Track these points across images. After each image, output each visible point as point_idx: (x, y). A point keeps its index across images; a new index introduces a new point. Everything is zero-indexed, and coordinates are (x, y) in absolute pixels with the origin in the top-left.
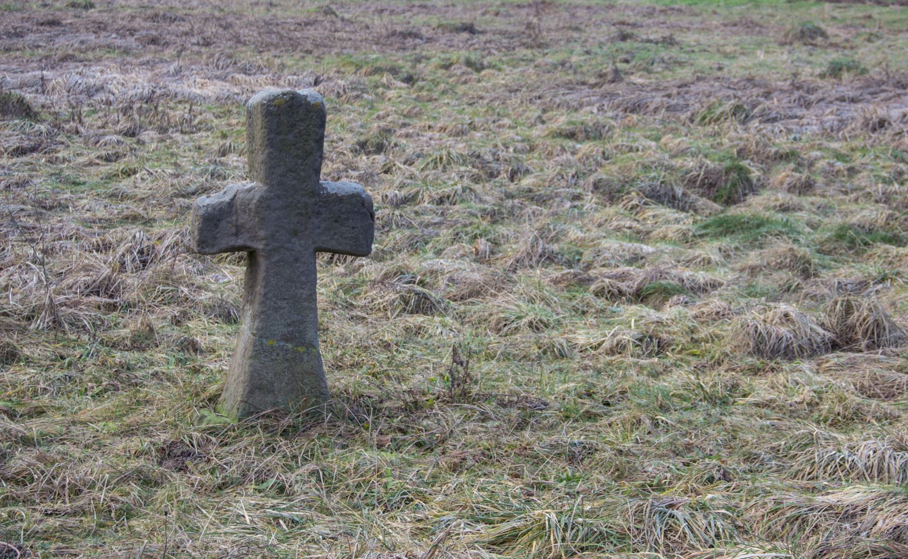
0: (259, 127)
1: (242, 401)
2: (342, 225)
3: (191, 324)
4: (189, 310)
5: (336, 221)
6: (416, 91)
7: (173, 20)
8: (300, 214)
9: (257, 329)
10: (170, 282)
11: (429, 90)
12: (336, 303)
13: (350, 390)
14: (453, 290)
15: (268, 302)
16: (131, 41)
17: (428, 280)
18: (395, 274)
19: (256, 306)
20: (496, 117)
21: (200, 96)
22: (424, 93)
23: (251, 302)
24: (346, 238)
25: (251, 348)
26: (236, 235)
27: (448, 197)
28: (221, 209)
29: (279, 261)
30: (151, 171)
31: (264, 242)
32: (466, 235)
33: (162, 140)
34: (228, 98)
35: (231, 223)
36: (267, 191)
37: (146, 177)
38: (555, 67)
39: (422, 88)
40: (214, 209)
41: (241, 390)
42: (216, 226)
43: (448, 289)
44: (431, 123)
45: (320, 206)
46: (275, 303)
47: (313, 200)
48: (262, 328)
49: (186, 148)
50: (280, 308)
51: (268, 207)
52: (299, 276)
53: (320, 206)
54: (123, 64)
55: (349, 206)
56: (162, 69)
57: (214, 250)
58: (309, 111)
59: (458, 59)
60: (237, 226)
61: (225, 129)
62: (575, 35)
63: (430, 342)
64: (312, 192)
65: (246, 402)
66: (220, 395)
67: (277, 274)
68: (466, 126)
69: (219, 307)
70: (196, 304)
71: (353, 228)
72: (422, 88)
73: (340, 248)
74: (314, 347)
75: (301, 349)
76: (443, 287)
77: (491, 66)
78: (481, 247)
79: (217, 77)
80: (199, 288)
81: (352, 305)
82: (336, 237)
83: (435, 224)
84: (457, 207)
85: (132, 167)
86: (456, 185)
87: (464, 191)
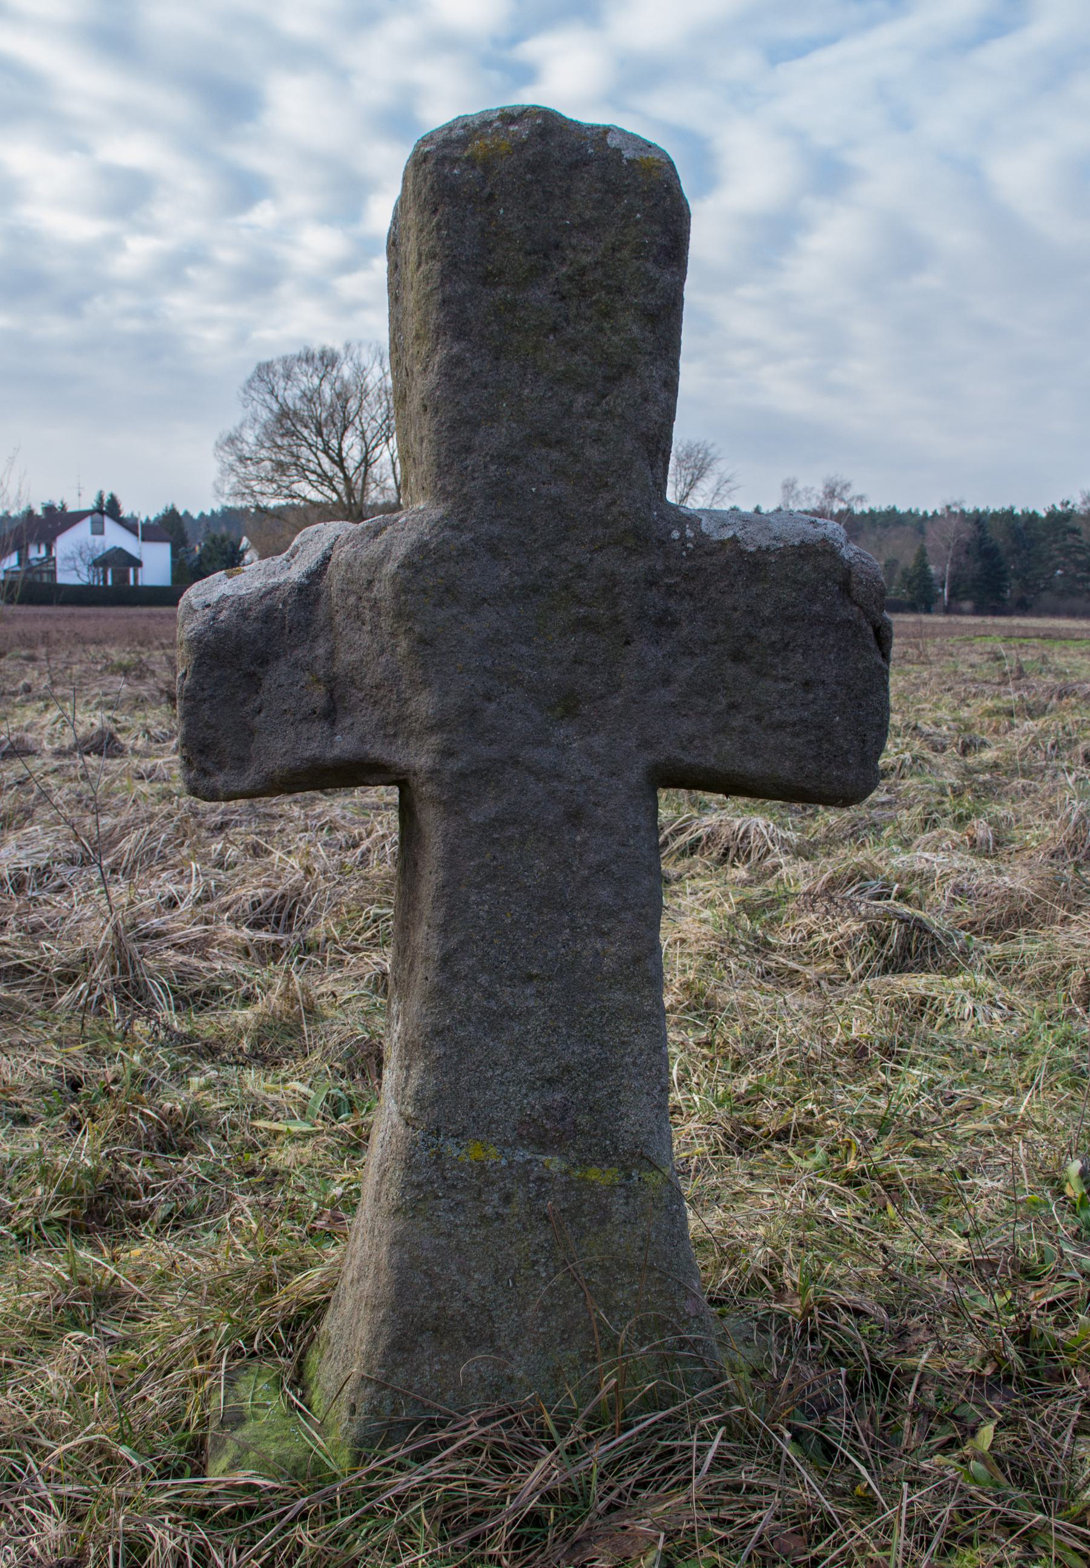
1: (365, 1381)
5: (738, 657)
8: (584, 624)
9: (418, 1099)
12: (733, 941)
14: (967, 911)
19: (415, 1005)
24: (780, 726)
26: (330, 714)
27: (893, 769)
28: (269, 616)
29: (499, 822)
31: (434, 741)
35: (308, 668)
36: (444, 523)
41: (363, 1332)
42: (253, 681)
43: (958, 909)
45: (670, 591)
46: (490, 995)
47: (640, 565)
48: (439, 1098)
51: (449, 591)
53: (670, 591)
57: (246, 783)
71: (807, 685)
73: (753, 766)
74: (654, 1167)
75: (600, 1176)
78: (980, 834)
82: (737, 721)
83: (883, 804)
84: (908, 782)
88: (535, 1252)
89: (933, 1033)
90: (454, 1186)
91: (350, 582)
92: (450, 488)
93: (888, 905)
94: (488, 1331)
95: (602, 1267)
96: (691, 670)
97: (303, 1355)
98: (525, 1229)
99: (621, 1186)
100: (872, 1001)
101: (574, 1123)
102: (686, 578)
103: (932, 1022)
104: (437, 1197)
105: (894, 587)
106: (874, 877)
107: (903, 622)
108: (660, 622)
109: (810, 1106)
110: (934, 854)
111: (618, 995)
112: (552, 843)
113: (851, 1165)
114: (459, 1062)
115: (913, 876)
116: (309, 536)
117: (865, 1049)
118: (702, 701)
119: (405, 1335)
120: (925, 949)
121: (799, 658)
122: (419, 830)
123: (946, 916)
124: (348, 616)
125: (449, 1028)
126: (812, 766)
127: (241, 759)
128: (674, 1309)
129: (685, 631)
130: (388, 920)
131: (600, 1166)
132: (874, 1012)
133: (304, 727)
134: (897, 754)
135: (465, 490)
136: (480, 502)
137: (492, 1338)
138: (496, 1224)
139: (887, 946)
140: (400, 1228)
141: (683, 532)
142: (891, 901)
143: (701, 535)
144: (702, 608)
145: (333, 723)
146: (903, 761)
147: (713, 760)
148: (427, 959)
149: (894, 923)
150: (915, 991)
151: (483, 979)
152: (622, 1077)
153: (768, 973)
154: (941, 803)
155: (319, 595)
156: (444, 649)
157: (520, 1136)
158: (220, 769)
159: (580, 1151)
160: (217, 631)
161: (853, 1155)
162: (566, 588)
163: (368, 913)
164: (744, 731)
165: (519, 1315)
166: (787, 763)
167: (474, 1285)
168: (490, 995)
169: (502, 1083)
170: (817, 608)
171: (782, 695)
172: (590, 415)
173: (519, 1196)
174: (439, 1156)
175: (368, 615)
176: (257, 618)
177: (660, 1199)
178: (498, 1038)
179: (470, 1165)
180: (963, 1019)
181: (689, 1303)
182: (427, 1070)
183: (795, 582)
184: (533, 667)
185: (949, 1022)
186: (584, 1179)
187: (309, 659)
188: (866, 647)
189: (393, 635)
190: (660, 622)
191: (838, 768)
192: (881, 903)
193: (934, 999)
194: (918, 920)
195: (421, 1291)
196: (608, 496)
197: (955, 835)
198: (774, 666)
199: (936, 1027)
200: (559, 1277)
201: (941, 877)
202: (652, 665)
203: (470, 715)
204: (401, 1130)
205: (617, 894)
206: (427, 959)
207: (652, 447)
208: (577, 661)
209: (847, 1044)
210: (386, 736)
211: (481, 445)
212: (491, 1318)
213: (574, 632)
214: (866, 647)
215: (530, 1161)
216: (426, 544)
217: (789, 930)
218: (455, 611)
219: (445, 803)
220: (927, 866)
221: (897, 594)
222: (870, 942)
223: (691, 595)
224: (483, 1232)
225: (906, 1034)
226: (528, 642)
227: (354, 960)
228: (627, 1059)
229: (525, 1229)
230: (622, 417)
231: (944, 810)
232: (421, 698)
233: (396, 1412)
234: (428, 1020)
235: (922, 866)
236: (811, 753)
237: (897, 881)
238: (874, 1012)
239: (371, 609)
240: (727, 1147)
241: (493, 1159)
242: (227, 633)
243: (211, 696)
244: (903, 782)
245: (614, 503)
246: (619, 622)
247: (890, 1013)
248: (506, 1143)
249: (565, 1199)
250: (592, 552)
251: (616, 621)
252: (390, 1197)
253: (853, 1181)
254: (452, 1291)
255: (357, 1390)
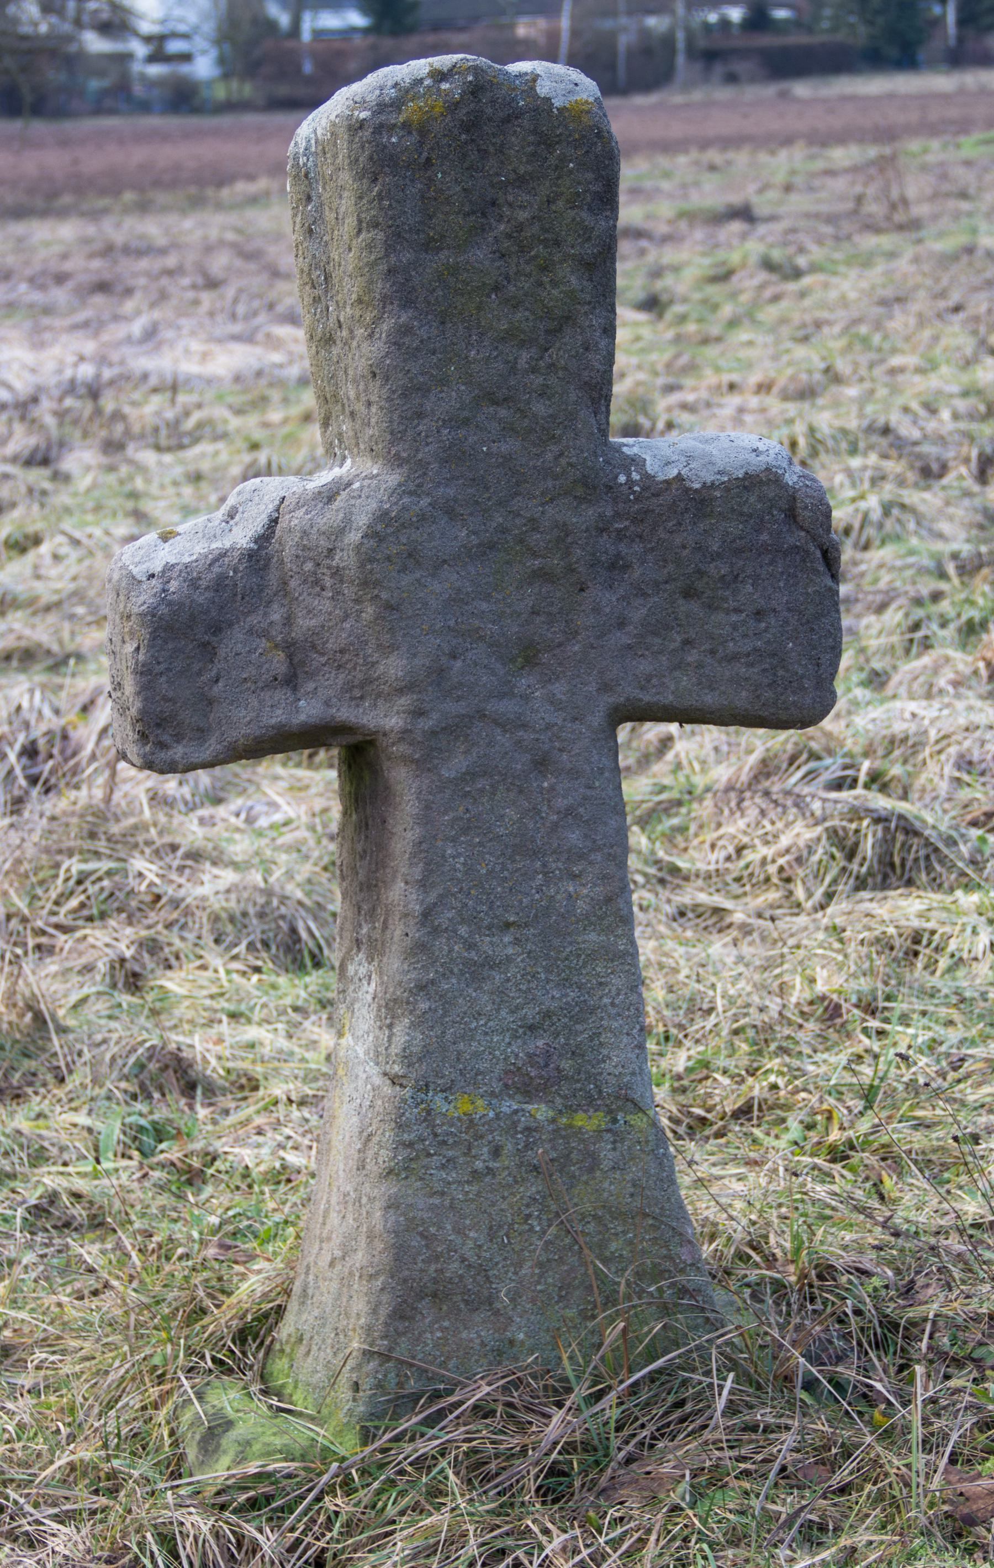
0: (351, 222)
1: (367, 1355)
2: (711, 607)
3: (173, 983)
4: (165, 936)
5: (689, 593)
6: (670, 325)
7: (140, 253)
8: (543, 575)
9: (407, 1057)
10: (101, 845)
11: (700, 320)
13: (780, 1243)
15: (441, 944)
16: (60, 295)
17: (896, 770)
18: (792, 760)
19: (394, 963)
20: (873, 356)
21: (200, 377)
22: (691, 327)
23: (375, 949)
24: (732, 658)
25: (387, 1135)
26: (291, 681)
28: (220, 584)
29: (470, 775)
30: (77, 534)
31: (404, 701)
32: (943, 625)
33: (112, 469)
34: (259, 374)
35: (265, 634)
36: (401, 490)
37: (64, 550)
38: (954, 258)
39: (682, 319)
40: (194, 583)
41: (360, 1305)
42: (208, 651)
43: (964, 794)
44: (735, 377)
45: (620, 535)
46: (470, 946)
48: (426, 1053)
49: (167, 480)
50: (491, 963)
51: (412, 556)
52: (555, 826)
53: (620, 535)
54: (37, 330)
55: (735, 528)
56: (118, 331)
57: (206, 754)
58: (546, 141)
59: (745, 258)
60: (290, 648)
61: (258, 435)
62: (965, 206)
63: (962, 979)
64: (584, 481)
65: (385, 1357)
66: (280, 1311)
67: (465, 831)
68: (818, 377)
69: (261, 915)
70: (188, 912)
71: (759, 614)
72: (682, 319)
73: (710, 699)
74: (638, 1108)
76: (944, 787)
77: (814, 268)
79: (236, 338)
80: (195, 856)
81: (674, 870)
82: (692, 657)
85: (31, 529)
86: (862, 497)
87: (886, 510)
88: (528, 1206)
89: (935, 981)
90: (444, 1143)
91: (305, 548)
92: (404, 455)
93: (856, 798)
94: (486, 1293)
95: (595, 1217)
96: (644, 611)
97: (264, 1365)
98: (516, 1182)
99: (608, 1131)
100: (841, 941)
101: (558, 1069)
102: (634, 521)
103: (931, 966)
104: (429, 1155)
105: (827, 12)
106: (830, 752)
107: (853, 98)
108: (612, 566)
109: (772, 1078)
110: (924, 703)
111: (593, 936)
112: (521, 792)
113: (835, 1136)
114: (444, 1016)
115: (892, 742)
116: (246, 496)
117: (838, 1007)
118: (658, 641)
119: (405, 1301)
120: (916, 860)
121: (749, 588)
122: (387, 788)
123: (946, 806)
124: (305, 582)
125: (432, 982)
126: (768, 694)
127: (200, 730)
128: (669, 1257)
129: (637, 573)
130: (100, 879)
131: (586, 1111)
132: (846, 956)
133: (266, 695)
134: (853, 500)
135: (420, 456)
136: (435, 466)
137: (490, 1300)
138: (487, 1179)
139: (857, 860)
140: (394, 1190)
141: (629, 476)
142: (859, 791)
143: (647, 476)
144: (652, 549)
145: (295, 689)
146: (866, 515)
147: (671, 698)
148: (406, 915)
149: (865, 823)
150: (903, 923)
151: (463, 930)
152: (602, 1019)
153: (682, 914)
154: (936, 597)
155: (269, 559)
156: (410, 613)
157: (506, 1085)
158: (178, 742)
159: (565, 1097)
160: (170, 604)
161: (836, 1126)
162: (521, 541)
163: (68, 870)
164: (700, 665)
165: (516, 1273)
166: (744, 693)
167: (470, 1244)
168: (470, 946)
169: (486, 1034)
170: (764, 537)
171: (735, 627)
172: (534, 370)
173: (509, 1147)
174: (429, 1112)
175: (328, 582)
176: (207, 588)
177: (647, 1142)
178: (480, 988)
179: (459, 1119)
180: (976, 959)
181: (684, 1250)
182: (413, 1025)
183: (741, 514)
184: (494, 623)
185: (956, 964)
186: (570, 1126)
187: (264, 625)
188: (816, 571)
189: (357, 601)
190: (612, 566)
191: (794, 693)
192: (845, 795)
193: (933, 932)
194: (901, 817)
195: (419, 1254)
196: (555, 449)
197: (962, 661)
198: (725, 599)
199: (938, 973)
200: (553, 1230)
201: (937, 742)
202: (607, 610)
203: (438, 674)
204: (388, 1090)
205: (586, 836)
206: (406, 915)
207: (595, 394)
208: (535, 612)
209: (811, 1003)
210: (352, 699)
211: (433, 411)
212: (487, 1277)
213: (530, 584)
214: (816, 571)
215: (516, 1112)
216: (386, 513)
217: (707, 846)
218: (418, 575)
219: (417, 762)
220: (912, 728)
221: (834, 29)
222: (833, 857)
223: (641, 537)
224: (475, 1188)
225: (893, 982)
226: (487, 598)
227: (70, 943)
228: (606, 1000)
229: (516, 1182)
230: (565, 369)
231: (942, 616)
232: (389, 661)
233: (400, 1385)
234: (413, 975)
235: (905, 726)
236: (766, 681)
237: (866, 755)
238: (846, 956)
239: (333, 575)
240: (675, 1132)
241: (481, 1111)
242: (181, 604)
243: (169, 670)
244: (868, 555)
245: (561, 454)
246: (573, 570)
247: (869, 956)
248: (493, 1094)
249: (554, 1148)
250: (543, 505)
251: (570, 570)
252: (380, 1160)
253: (838, 1155)
254: (449, 1251)
255: (359, 1367)
